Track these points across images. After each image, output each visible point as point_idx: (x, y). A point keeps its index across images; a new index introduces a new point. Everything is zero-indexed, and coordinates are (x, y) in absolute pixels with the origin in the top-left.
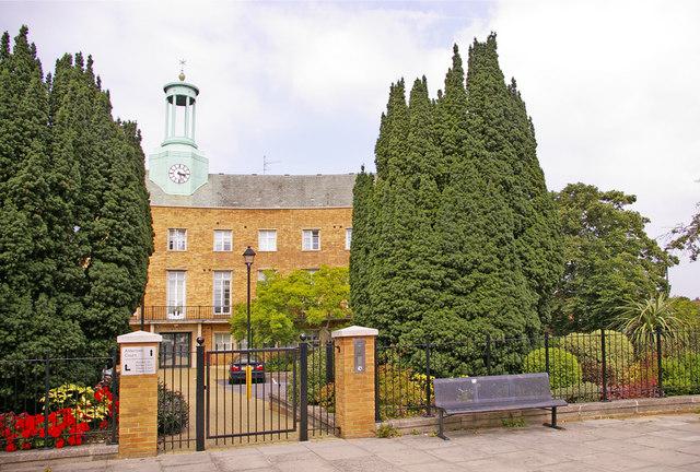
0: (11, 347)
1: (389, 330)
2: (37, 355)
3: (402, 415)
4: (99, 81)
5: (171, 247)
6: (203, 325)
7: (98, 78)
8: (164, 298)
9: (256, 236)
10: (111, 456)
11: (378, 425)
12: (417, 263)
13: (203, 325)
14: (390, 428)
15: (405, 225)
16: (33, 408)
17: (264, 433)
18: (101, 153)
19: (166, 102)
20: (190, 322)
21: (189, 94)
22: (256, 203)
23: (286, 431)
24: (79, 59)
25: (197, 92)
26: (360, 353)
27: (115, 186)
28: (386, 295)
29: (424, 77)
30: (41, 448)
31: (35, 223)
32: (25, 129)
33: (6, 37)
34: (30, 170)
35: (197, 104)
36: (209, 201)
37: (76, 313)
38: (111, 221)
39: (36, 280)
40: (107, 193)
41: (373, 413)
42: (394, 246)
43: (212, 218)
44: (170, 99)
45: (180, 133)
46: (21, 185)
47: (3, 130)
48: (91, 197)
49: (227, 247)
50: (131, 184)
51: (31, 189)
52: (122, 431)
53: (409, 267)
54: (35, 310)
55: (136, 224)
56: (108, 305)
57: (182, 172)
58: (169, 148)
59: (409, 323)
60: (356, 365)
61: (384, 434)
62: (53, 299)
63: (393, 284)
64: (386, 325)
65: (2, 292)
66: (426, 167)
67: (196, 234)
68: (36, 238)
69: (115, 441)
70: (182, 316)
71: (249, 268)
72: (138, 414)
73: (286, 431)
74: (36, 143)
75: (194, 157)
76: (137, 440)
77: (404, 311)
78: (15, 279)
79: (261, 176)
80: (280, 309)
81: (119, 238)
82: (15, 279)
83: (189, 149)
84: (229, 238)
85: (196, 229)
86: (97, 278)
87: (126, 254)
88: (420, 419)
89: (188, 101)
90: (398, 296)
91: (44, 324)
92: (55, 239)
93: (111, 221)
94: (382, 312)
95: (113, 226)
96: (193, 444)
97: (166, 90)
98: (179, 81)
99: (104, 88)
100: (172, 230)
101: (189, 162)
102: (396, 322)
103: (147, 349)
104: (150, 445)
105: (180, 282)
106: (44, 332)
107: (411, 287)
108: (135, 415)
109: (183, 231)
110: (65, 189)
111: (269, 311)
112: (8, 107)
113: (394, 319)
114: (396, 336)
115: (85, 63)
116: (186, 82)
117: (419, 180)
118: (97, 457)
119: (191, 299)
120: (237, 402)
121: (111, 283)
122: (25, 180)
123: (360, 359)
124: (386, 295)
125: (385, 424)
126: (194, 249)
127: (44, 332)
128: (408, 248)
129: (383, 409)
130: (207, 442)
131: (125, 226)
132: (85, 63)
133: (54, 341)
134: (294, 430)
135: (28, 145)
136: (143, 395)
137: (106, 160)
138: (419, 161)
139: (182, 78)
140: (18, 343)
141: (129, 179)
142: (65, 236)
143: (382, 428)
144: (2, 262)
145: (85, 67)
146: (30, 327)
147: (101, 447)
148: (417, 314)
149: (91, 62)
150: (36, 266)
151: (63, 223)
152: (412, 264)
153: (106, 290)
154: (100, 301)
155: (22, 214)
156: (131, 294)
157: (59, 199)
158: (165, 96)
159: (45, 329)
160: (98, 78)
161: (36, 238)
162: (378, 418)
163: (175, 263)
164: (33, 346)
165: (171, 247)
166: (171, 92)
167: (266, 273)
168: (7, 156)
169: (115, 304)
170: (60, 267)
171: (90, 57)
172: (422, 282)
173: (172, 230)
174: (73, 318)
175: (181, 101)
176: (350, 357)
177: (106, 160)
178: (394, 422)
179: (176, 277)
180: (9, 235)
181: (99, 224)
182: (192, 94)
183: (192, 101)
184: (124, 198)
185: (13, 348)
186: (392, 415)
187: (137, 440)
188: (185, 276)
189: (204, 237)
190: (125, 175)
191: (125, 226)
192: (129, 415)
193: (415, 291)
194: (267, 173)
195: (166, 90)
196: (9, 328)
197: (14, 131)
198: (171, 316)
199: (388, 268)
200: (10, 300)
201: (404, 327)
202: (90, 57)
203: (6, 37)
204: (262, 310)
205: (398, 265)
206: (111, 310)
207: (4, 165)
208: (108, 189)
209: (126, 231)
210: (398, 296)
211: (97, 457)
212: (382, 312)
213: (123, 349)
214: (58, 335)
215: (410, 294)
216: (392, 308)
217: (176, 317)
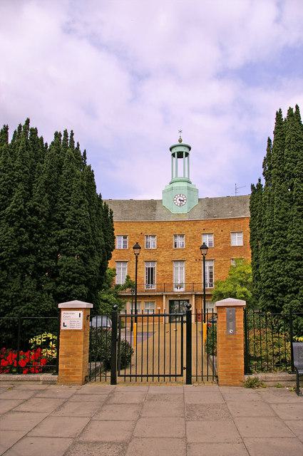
0: (8, 309)
1: (275, 301)
2: (25, 315)
3: (270, 370)
4: (78, 145)
5: (176, 246)
6: (196, 295)
7: (78, 143)
8: (172, 278)
9: (200, 236)
10: (53, 383)
11: (247, 377)
12: (292, 248)
13: (196, 295)
14: (256, 380)
15: (282, 219)
16: (26, 347)
17: (148, 376)
18: (65, 188)
19: (170, 156)
20: (188, 293)
21: (184, 150)
22: (229, 215)
23: (176, 376)
24: (66, 132)
25: (190, 148)
26: (231, 319)
27: (71, 208)
28: (270, 274)
29: (280, 110)
30: (14, 373)
31: (22, 234)
32: (15, 177)
33: (6, 128)
34: (15, 202)
35: (190, 156)
36: (198, 215)
37: (50, 288)
38: (69, 230)
39: (24, 268)
40: (67, 213)
41: (242, 367)
42: (274, 236)
43: (200, 226)
44: (173, 155)
45: (180, 175)
46: (11, 211)
47: (2, 179)
48: (57, 216)
49: (210, 244)
50: (83, 206)
51: (16, 213)
52: (61, 366)
53: (286, 252)
54: (23, 287)
55: (85, 231)
56: (71, 283)
57: (182, 199)
58: (175, 185)
59: (289, 296)
60: (228, 328)
61: (251, 385)
62: (35, 280)
63: (275, 266)
64: (272, 297)
65: (0, 275)
66: (298, 173)
67: (190, 238)
68: (21, 243)
69: (57, 373)
70: (182, 290)
71: (137, 257)
72: (73, 354)
73: (176, 376)
74: (20, 185)
75: (189, 188)
76: (71, 374)
77: (284, 286)
78: (10, 268)
79: (233, 197)
80: (242, 284)
81: (75, 240)
82: (10, 268)
83: (185, 184)
84: (212, 238)
85: (190, 234)
86: (61, 266)
87: (80, 250)
88: (284, 375)
89: (184, 154)
90: (279, 275)
91: (27, 295)
92: (35, 242)
93: (69, 230)
94: (268, 287)
95: (71, 233)
96: (109, 379)
97: (171, 149)
98: (178, 143)
99: (82, 150)
100: (175, 236)
101: (185, 192)
102: (280, 294)
103: (77, 313)
104: (77, 377)
105: (181, 268)
106: (28, 300)
107: (287, 267)
108: (69, 357)
109: (182, 236)
110: (38, 211)
111: (235, 286)
112: (5, 166)
113: (278, 292)
114: (281, 305)
115: (69, 135)
116: (182, 143)
117: (293, 184)
118: (45, 382)
119: (188, 278)
120: (145, 347)
121: (70, 269)
122: (13, 207)
123: (231, 324)
124: (270, 274)
125: (253, 376)
126: (189, 246)
127: (28, 300)
128: (285, 237)
129: (251, 362)
130: (193, 379)
131: (78, 233)
132: (69, 135)
133: (36, 306)
134: (182, 375)
135: (16, 187)
136: (74, 344)
137: (68, 192)
138: (292, 169)
139: (180, 141)
140: (13, 307)
141: (82, 202)
142: (41, 240)
143: (249, 379)
144: (1, 258)
145: (69, 138)
146: (20, 297)
147: (48, 376)
148: (295, 288)
149: (72, 134)
150: (22, 260)
151: (40, 232)
152: (288, 249)
153: (68, 274)
154: (65, 281)
155: (12, 229)
156: (86, 276)
157: (35, 218)
158: (171, 153)
159: (29, 298)
160: (78, 143)
161: (21, 243)
162: (247, 371)
163: (178, 256)
164: (22, 309)
165: (176, 246)
166: (174, 151)
167: (236, 260)
168: (5, 194)
169: (74, 283)
170: (39, 260)
171: (72, 131)
172: (296, 263)
173: (175, 236)
174: (49, 292)
175: (180, 155)
176: (223, 322)
177: (68, 192)
178: (261, 376)
179: (179, 265)
180: (4, 241)
181: (62, 233)
182: (187, 150)
183: (187, 154)
184: (77, 214)
185: (10, 310)
186: (262, 370)
187: (71, 374)
188: (184, 265)
189: (196, 238)
190: (79, 200)
191: (78, 233)
192: (65, 356)
193: (291, 270)
194: (238, 195)
195: (171, 149)
196: (6, 297)
197: (8, 179)
198: (176, 290)
199: (271, 254)
200: (7, 280)
201: (285, 299)
202: (72, 131)
203: (6, 128)
204: (230, 285)
205: (278, 250)
206: (72, 287)
207: (3, 200)
208: (68, 209)
209: (79, 236)
210: (279, 275)
211: (45, 382)
212: (268, 287)
213: (63, 312)
214: (37, 302)
215: (288, 273)
216: (276, 284)
217: (179, 290)
